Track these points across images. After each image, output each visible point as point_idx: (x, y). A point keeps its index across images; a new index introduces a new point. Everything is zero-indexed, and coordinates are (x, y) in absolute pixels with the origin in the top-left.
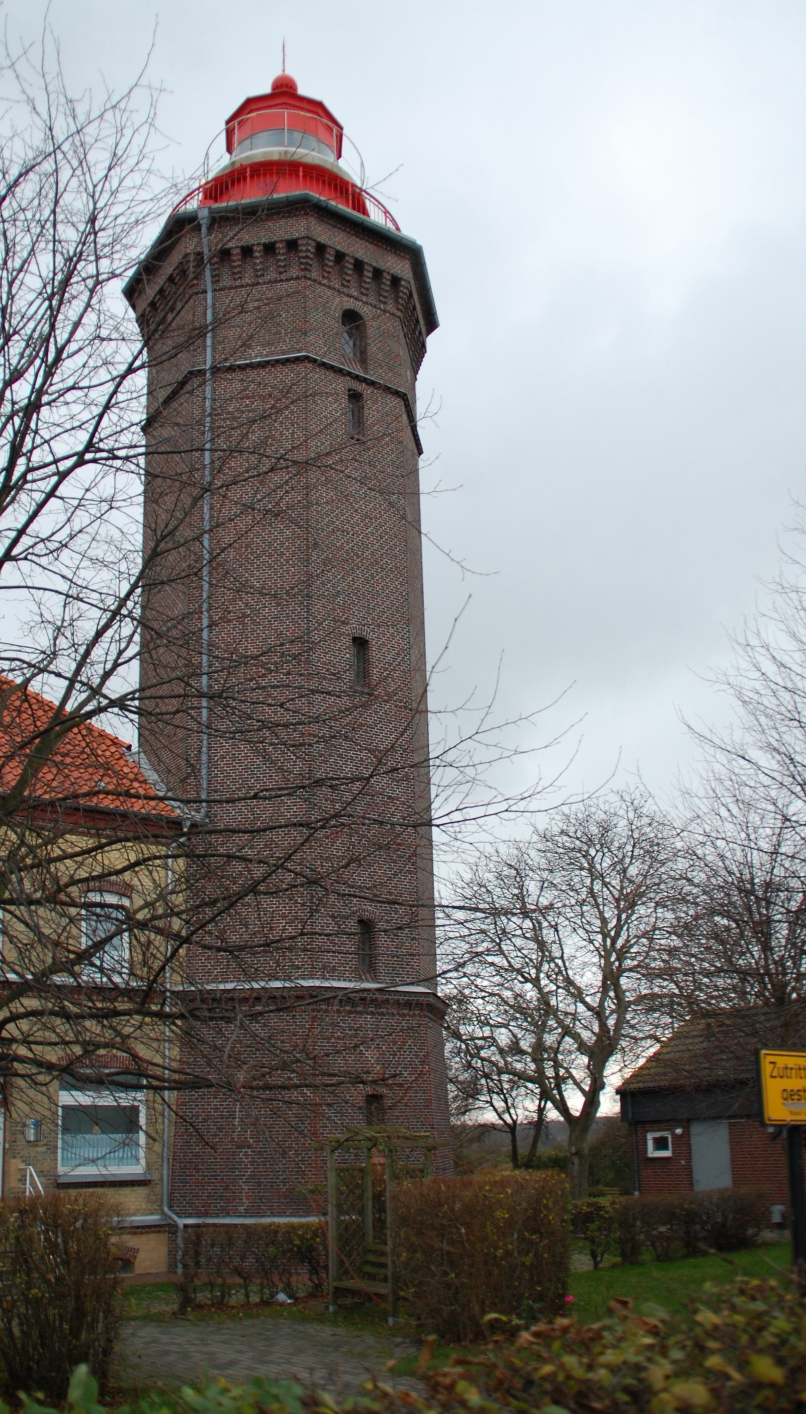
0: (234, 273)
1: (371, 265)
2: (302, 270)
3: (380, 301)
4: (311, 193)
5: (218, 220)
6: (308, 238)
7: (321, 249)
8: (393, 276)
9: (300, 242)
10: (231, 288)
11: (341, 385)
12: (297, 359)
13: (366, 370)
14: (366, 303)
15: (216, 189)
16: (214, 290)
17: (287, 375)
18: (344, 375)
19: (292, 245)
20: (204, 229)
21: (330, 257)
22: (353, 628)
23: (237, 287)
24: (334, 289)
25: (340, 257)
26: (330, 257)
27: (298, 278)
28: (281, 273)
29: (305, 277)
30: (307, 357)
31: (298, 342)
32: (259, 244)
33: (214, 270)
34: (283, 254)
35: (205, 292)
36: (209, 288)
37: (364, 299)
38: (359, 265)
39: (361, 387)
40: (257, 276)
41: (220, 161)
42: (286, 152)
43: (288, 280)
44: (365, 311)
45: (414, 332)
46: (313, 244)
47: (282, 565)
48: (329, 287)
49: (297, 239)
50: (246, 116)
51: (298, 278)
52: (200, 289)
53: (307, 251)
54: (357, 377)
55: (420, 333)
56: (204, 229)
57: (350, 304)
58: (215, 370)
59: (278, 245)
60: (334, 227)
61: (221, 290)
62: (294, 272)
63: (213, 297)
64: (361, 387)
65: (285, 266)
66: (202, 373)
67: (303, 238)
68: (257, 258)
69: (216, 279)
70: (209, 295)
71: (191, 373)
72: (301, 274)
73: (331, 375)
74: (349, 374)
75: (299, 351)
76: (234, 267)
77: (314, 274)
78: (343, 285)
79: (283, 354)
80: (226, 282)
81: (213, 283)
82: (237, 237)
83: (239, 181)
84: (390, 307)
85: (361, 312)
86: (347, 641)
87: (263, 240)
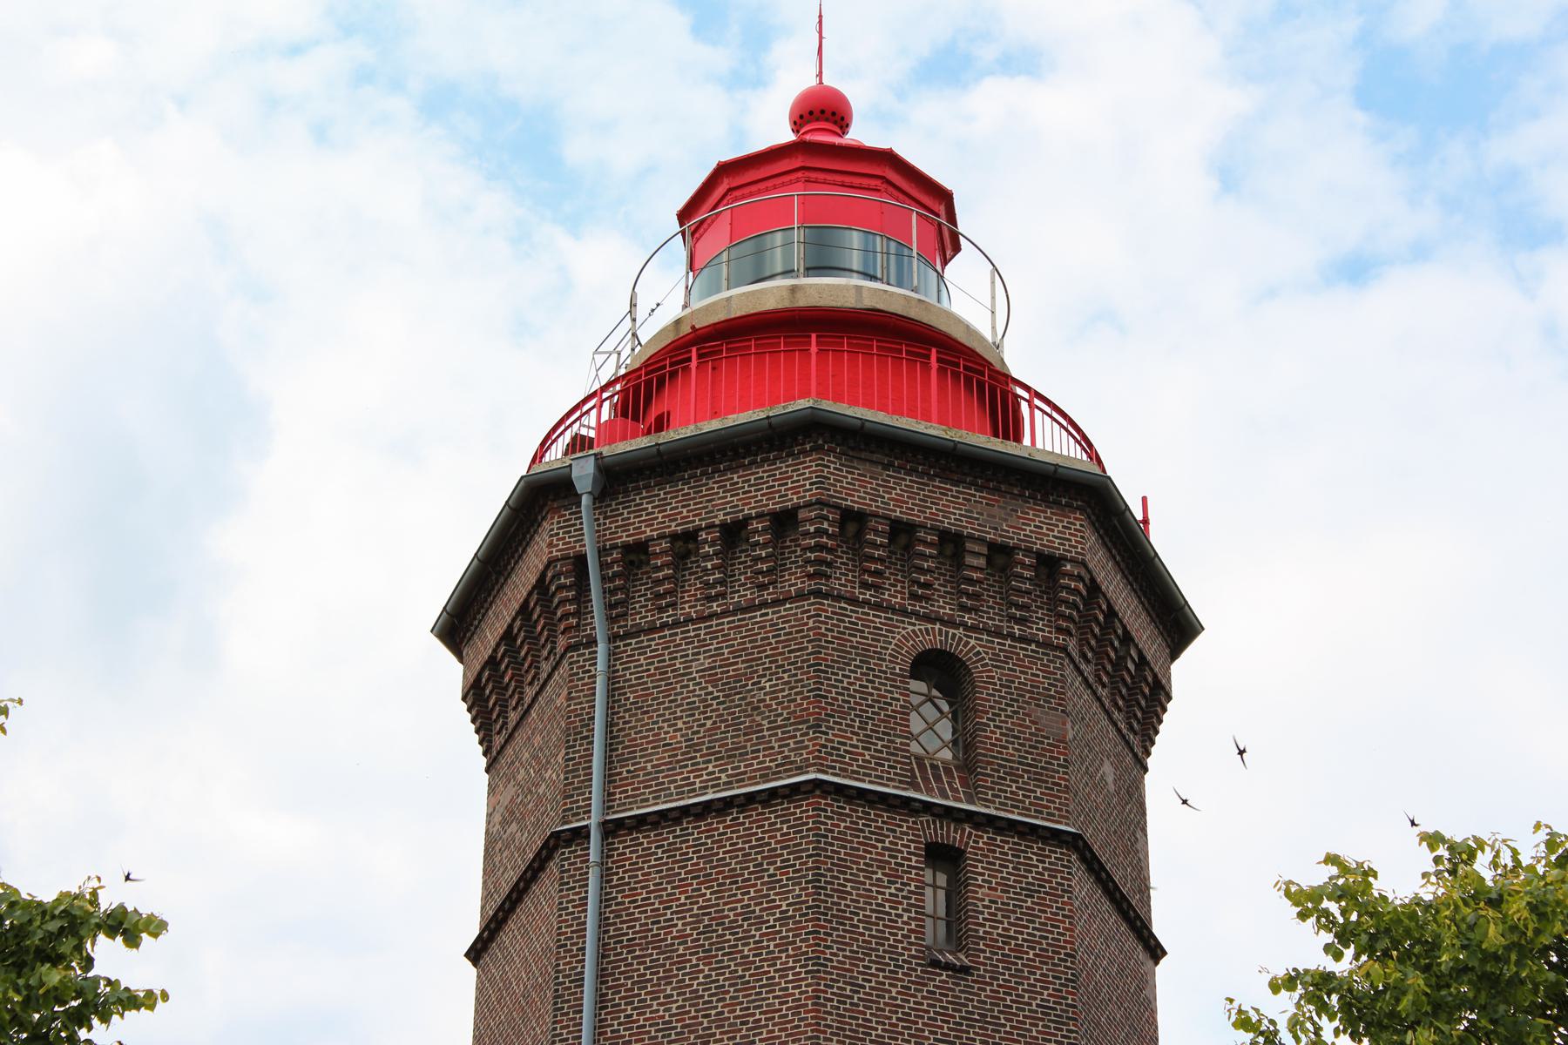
0: (658, 596)
1: (981, 540)
2: (810, 576)
3: (1011, 618)
4: (827, 405)
5: (617, 479)
7: (852, 521)
9: (802, 514)
10: (652, 629)
11: (907, 838)
14: (974, 628)
16: (613, 638)
17: (773, 828)
19: (784, 521)
21: (877, 537)
23: (664, 626)
24: (891, 608)
25: (902, 531)
26: (877, 537)
27: (801, 596)
28: (762, 587)
30: (817, 783)
31: (801, 747)
32: (711, 526)
33: (613, 592)
34: (765, 546)
35: (592, 642)
36: (600, 634)
37: (969, 619)
38: (952, 543)
40: (710, 599)
41: (668, 298)
42: (794, 290)
43: (776, 602)
44: (971, 646)
45: (1119, 664)
48: (878, 607)
49: (797, 508)
50: (727, 196)
51: (801, 596)
53: (820, 532)
55: (1142, 662)
60: (886, 467)
61: (627, 635)
62: (794, 581)
64: (954, 835)
65: (770, 571)
66: (581, 834)
67: (808, 505)
68: (707, 557)
70: (601, 649)
75: (801, 770)
76: (658, 582)
77: (841, 581)
78: (914, 596)
79: (765, 778)
80: (641, 615)
81: (612, 620)
82: (655, 515)
83: (673, 374)
84: (1041, 628)
85: (961, 651)
87: (720, 517)
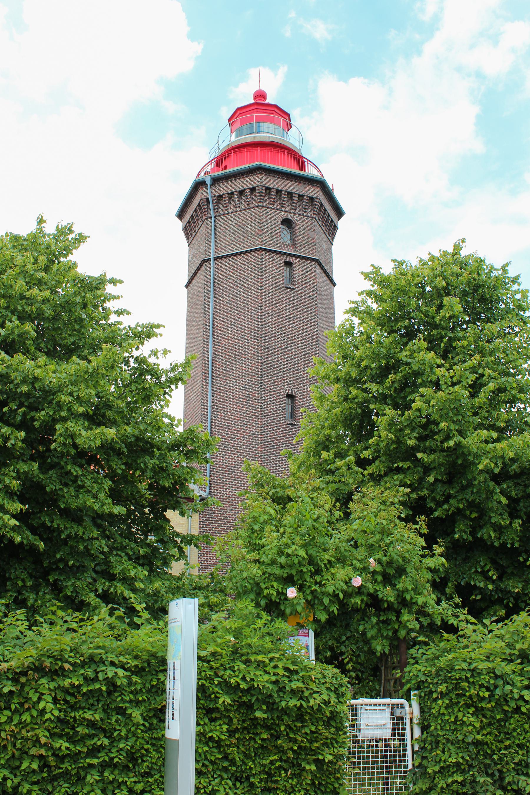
4: (262, 163)
5: (216, 181)
6: (261, 186)
7: (268, 189)
8: (310, 197)
12: (256, 250)
13: (295, 250)
15: (220, 161)
18: (282, 255)
20: (209, 186)
21: (273, 193)
22: (287, 389)
26: (273, 193)
27: (257, 207)
28: (248, 205)
29: (260, 206)
30: (261, 248)
38: (290, 195)
39: (290, 259)
44: (294, 218)
46: (264, 189)
47: (248, 360)
48: (274, 209)
50: (240, 115)
51: (257, 207)
52: (208, 216)
53: (261, 192)
54: (289, 255)
56: (209, 186)
57: (286, 216)
58: (216, 259)
59: (246, 191)
62: (255, 203)
63: (215, 220)
64: (290, 259)
66: (209, 260)
69: (216, 210)
70: (213, 219)
71: (204, 260)
72: (259, 204)
73: (275, 256)
74: (285, 253)
75: (257, 245)
77: (265, 204)
78: (282, 207)
79: (249, 247)
80: (222, 211)
82: (224, 188)
84: (310, 214)
85: (292, 219)
86: (283, 397)
87: (239, 189)
